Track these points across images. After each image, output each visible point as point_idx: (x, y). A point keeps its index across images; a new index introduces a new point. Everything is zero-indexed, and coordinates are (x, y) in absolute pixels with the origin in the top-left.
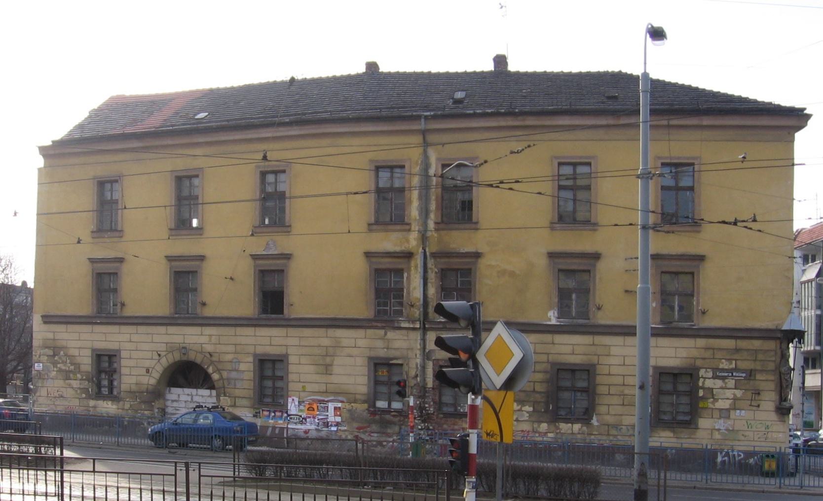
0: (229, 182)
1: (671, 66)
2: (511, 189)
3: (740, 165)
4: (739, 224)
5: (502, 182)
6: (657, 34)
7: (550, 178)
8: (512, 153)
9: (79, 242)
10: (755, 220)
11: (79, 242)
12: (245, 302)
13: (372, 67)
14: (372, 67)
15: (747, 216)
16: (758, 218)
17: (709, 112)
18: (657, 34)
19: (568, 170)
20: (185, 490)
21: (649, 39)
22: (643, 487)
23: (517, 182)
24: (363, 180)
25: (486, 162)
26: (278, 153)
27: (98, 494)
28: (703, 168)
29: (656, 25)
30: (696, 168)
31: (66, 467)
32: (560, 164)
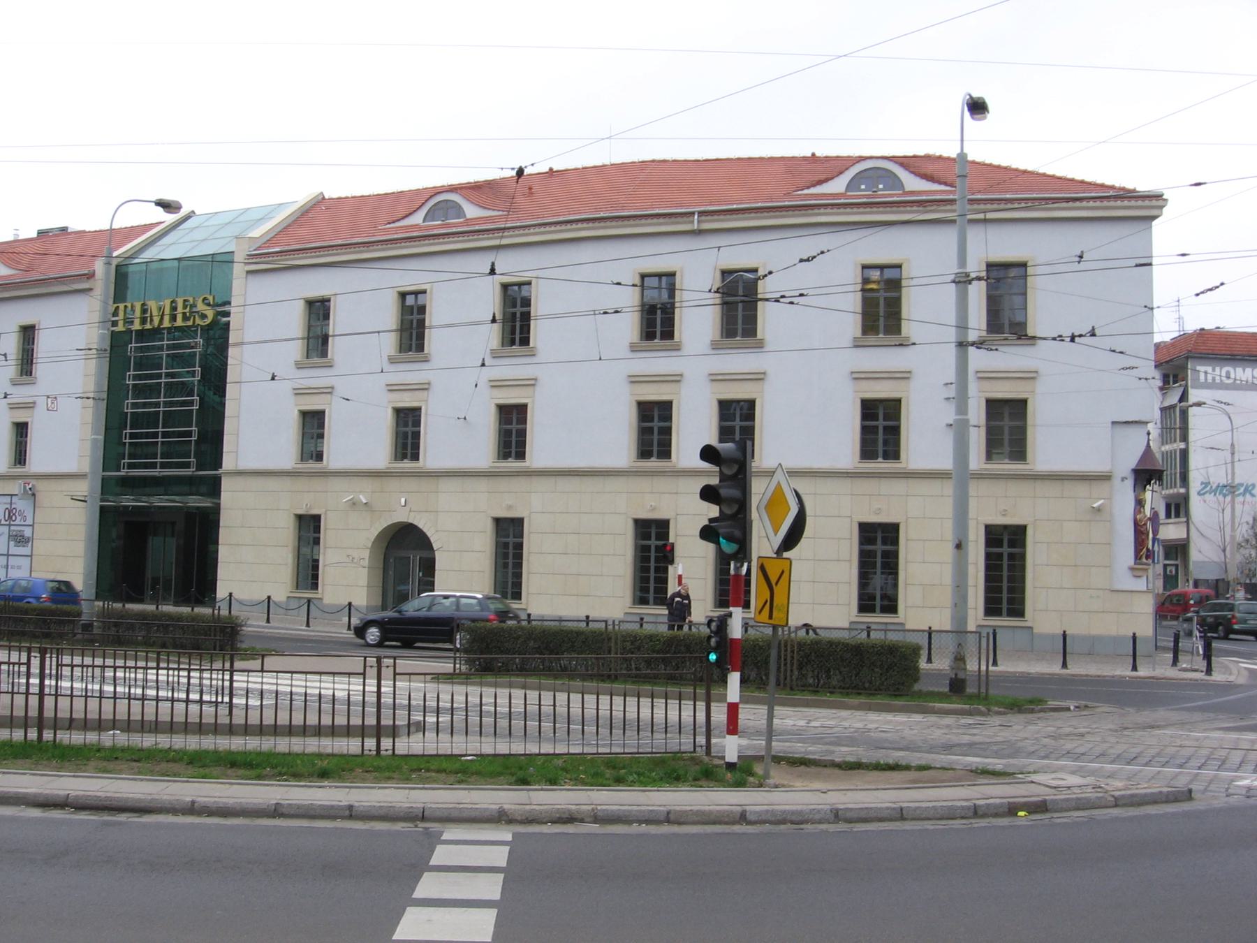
0: (463, 302)
1: (989, 145)
2: (792, 303)
3: (1076, 267)
4: (1077, 339)
5: (783, 297)
6: (977, 107)
7: (684, 304)
8: (801, 261)
9: (273, 379)
10: (1093, 335)
11: (273, 379)
12: (480, 447)
13: (813, 155)
14: (813, 155)
15: (1086, 329)
16: (1097, 332)
17: (1116, 198)
18: (977, 107)
19: (875, 275)
20: (375, 689)
21: (967, 114)
22: (961, 675)
23: (801, 295)
24: (629, 299)
25: (770, 273)
26: (513, 266)
27: (251, 702)
28: (684, 304)
29: (975, 95)
30: (1030, 270)
31: (237, 665)
32: (864, 267)
